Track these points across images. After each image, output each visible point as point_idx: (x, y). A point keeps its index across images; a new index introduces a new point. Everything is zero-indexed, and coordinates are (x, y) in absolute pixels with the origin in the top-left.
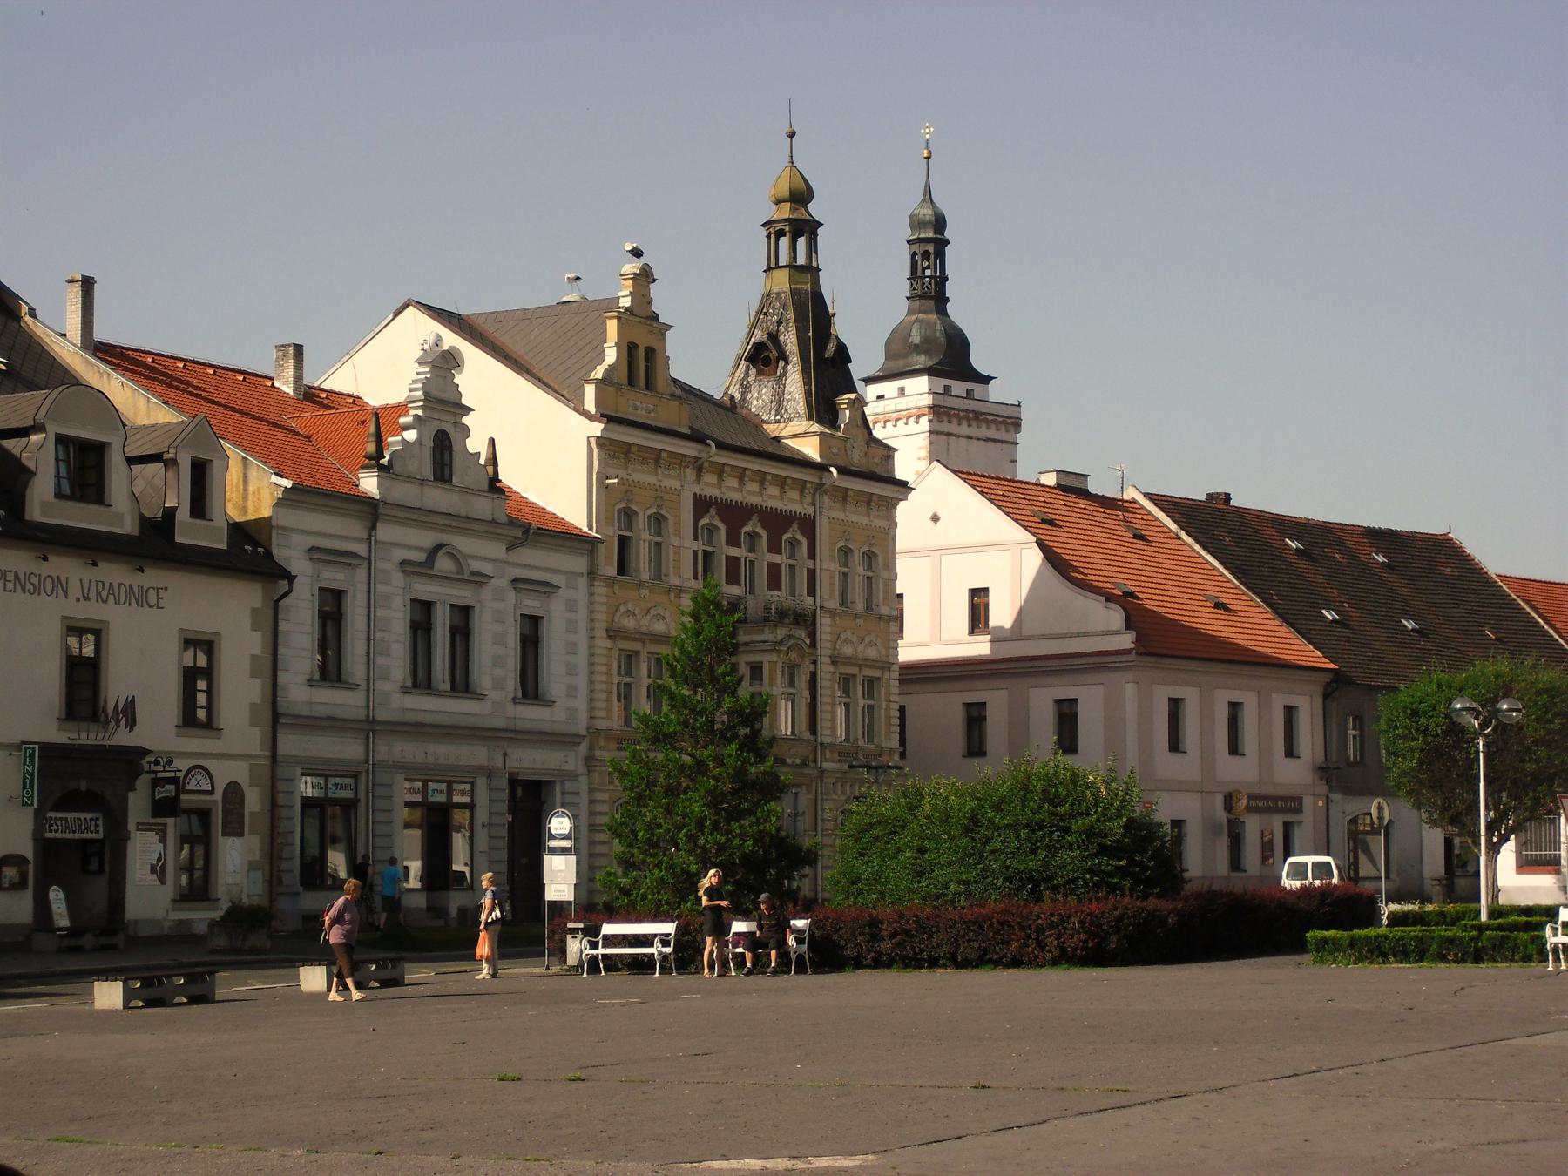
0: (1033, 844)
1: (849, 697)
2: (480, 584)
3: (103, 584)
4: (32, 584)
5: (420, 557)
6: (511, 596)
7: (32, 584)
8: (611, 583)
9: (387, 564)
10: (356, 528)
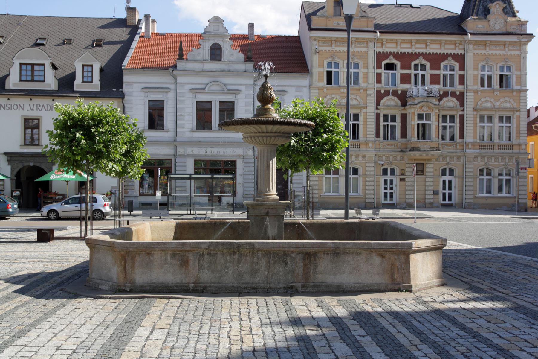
1: (510, 123)
2: (237, 94)
3: (40, 106)
6: (191, 95)
8: (320, 89)
9: (184, 90)
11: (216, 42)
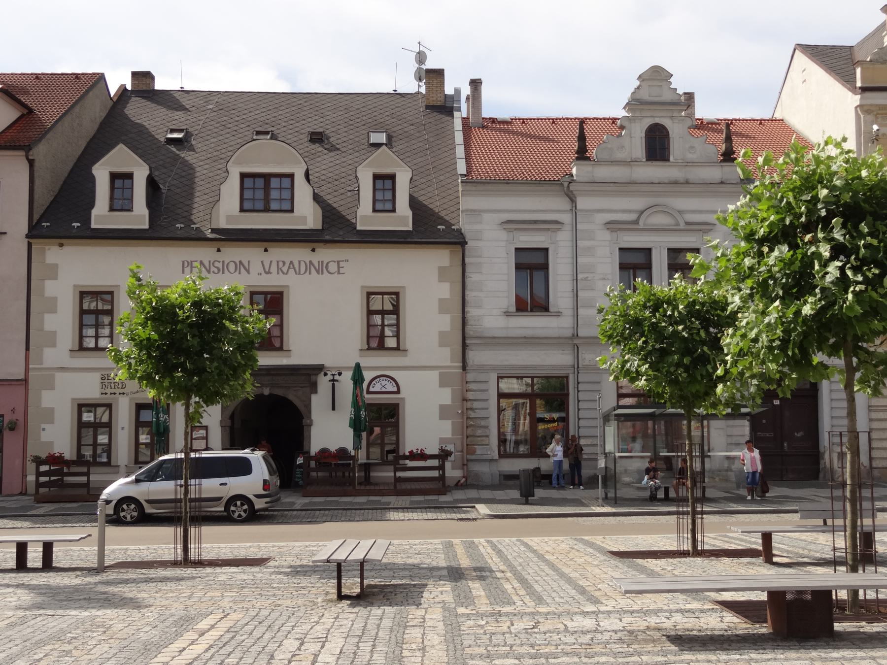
0: (743, 396)
3: (284, 263)
4: (216, 267)
5: (632, 217)
6: (606, 235)
7: (216, 267)
10: (562, 203)
11: (657, 120)
